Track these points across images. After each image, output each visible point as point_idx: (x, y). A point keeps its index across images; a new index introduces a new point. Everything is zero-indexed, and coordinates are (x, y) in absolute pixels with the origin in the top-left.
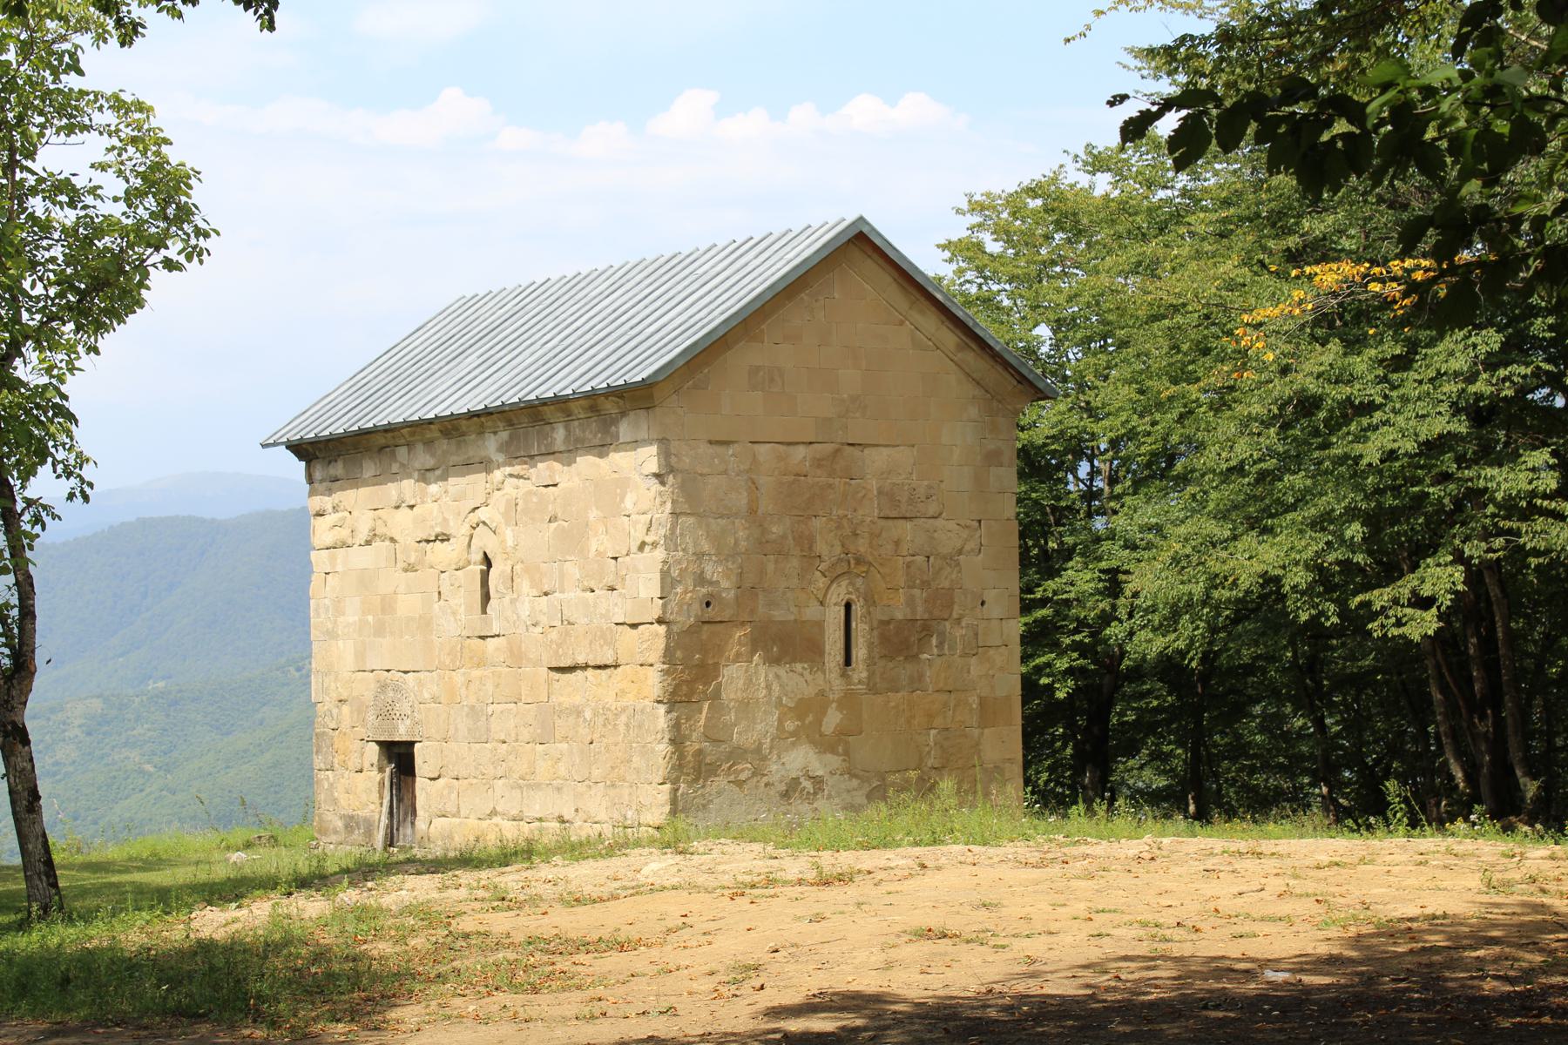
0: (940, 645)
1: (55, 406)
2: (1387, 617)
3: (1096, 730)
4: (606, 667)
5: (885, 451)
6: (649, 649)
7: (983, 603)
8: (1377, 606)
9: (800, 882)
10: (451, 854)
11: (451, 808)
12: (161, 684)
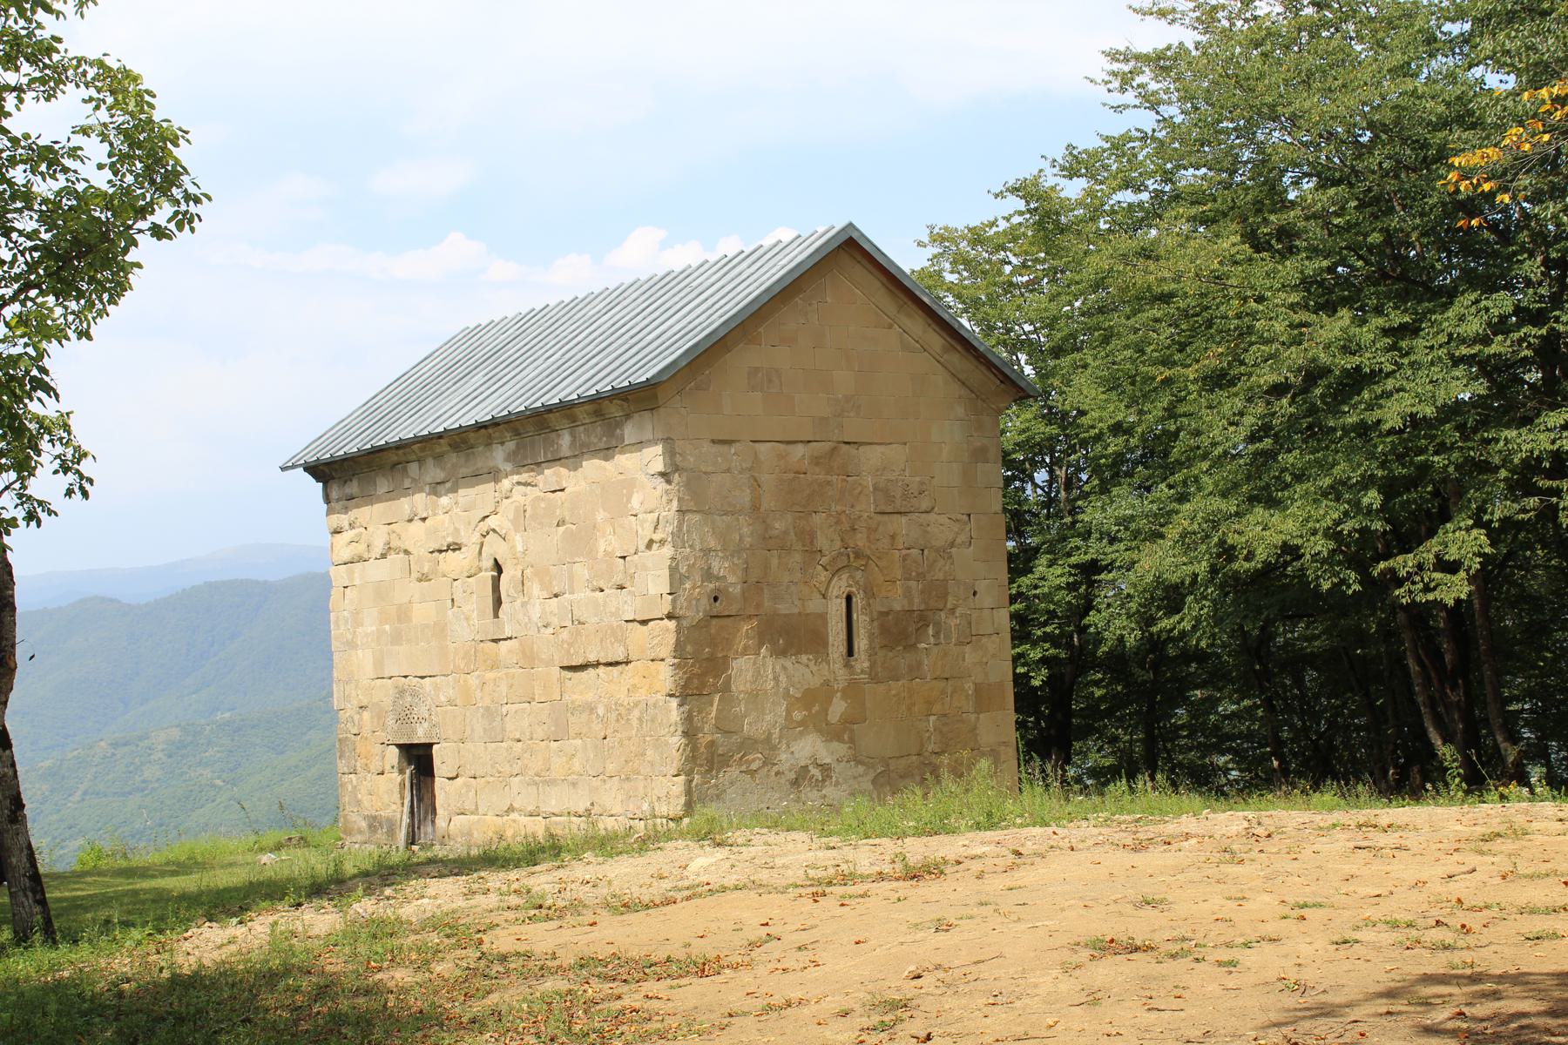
0: (937, 635)
1: (33, 379)
2: (1414, 583)
3: (1059, 716)
4: (617, 663)
5: (879, 449)
8: (1403, 573)
9: (881, 876)
10: (474, 852)
11: (469, 806)
12: (227, 715)
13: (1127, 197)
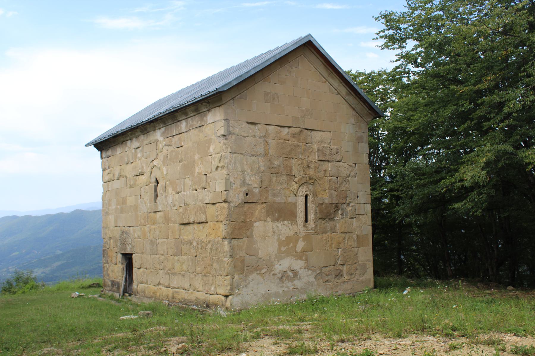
0: (342, 214)
4: (202, 223)
5: (320, 133)
6: (220, 214)
7: (358, 197)
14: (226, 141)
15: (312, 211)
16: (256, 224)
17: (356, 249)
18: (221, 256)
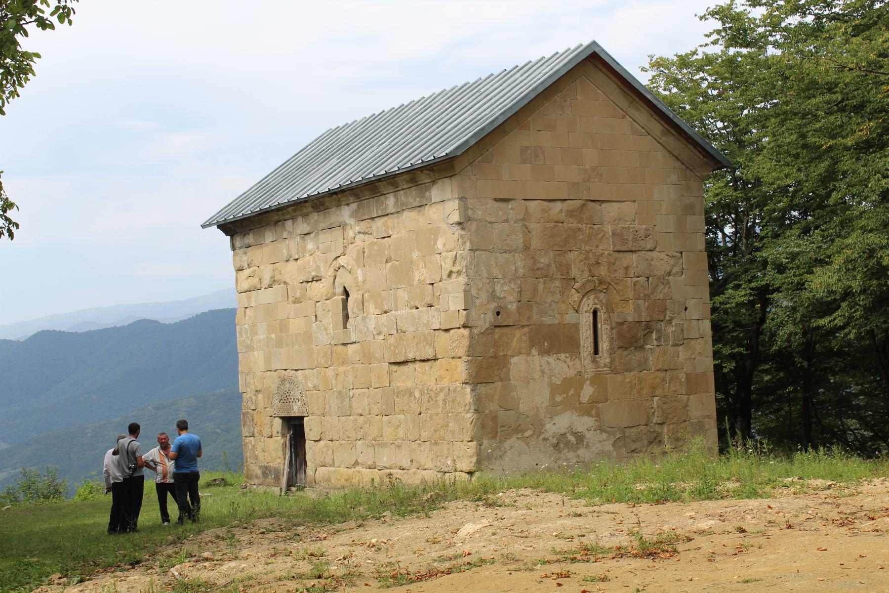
4: (428, 360)
6: (458, 347)
7: (686, 309)
11: (329, 460)
12: (223, 390)
13: (794, 20)
14: (463, 232)
15: (605, 336)
16: (514, 360)
17: (686, 397)
18: (460, 410)
